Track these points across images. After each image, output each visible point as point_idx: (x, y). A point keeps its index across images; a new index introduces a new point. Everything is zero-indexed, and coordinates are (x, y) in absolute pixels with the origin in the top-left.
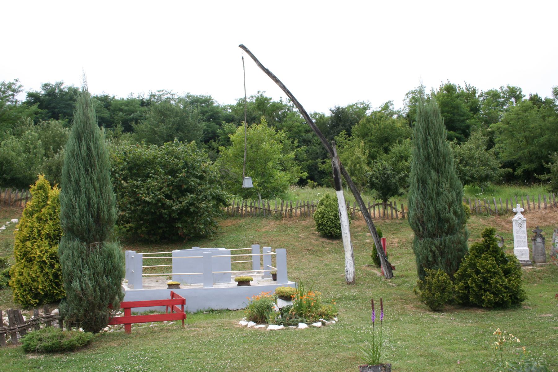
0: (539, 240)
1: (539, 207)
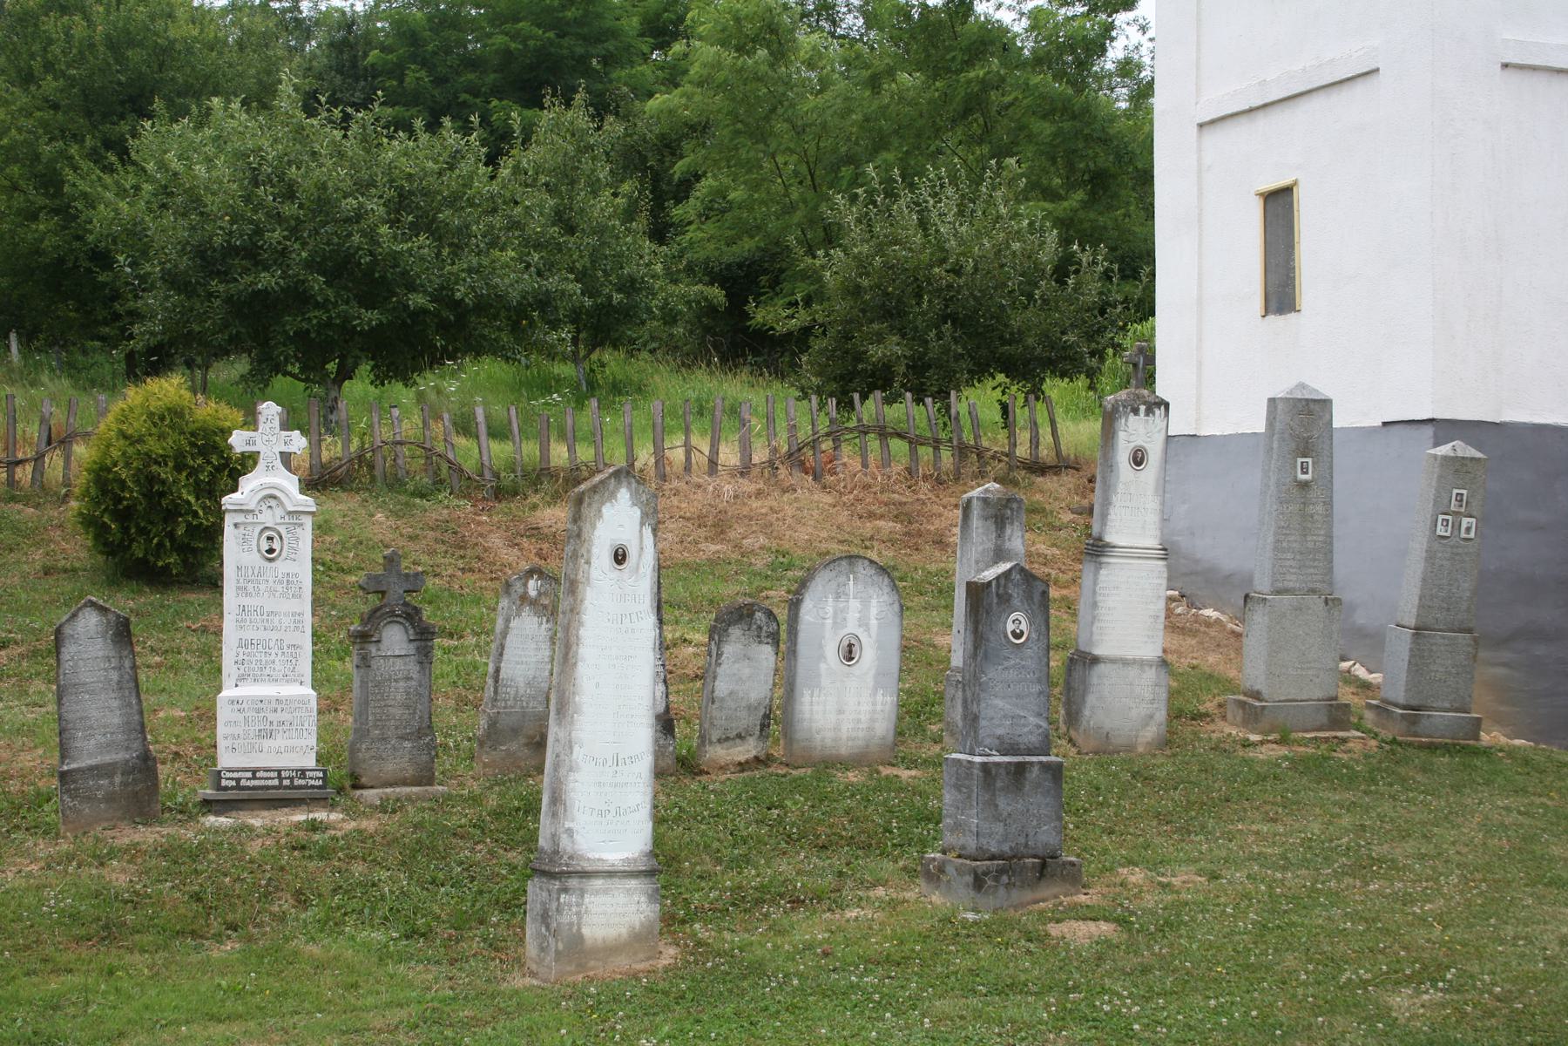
0: (395, 639)
1: (713, 463)
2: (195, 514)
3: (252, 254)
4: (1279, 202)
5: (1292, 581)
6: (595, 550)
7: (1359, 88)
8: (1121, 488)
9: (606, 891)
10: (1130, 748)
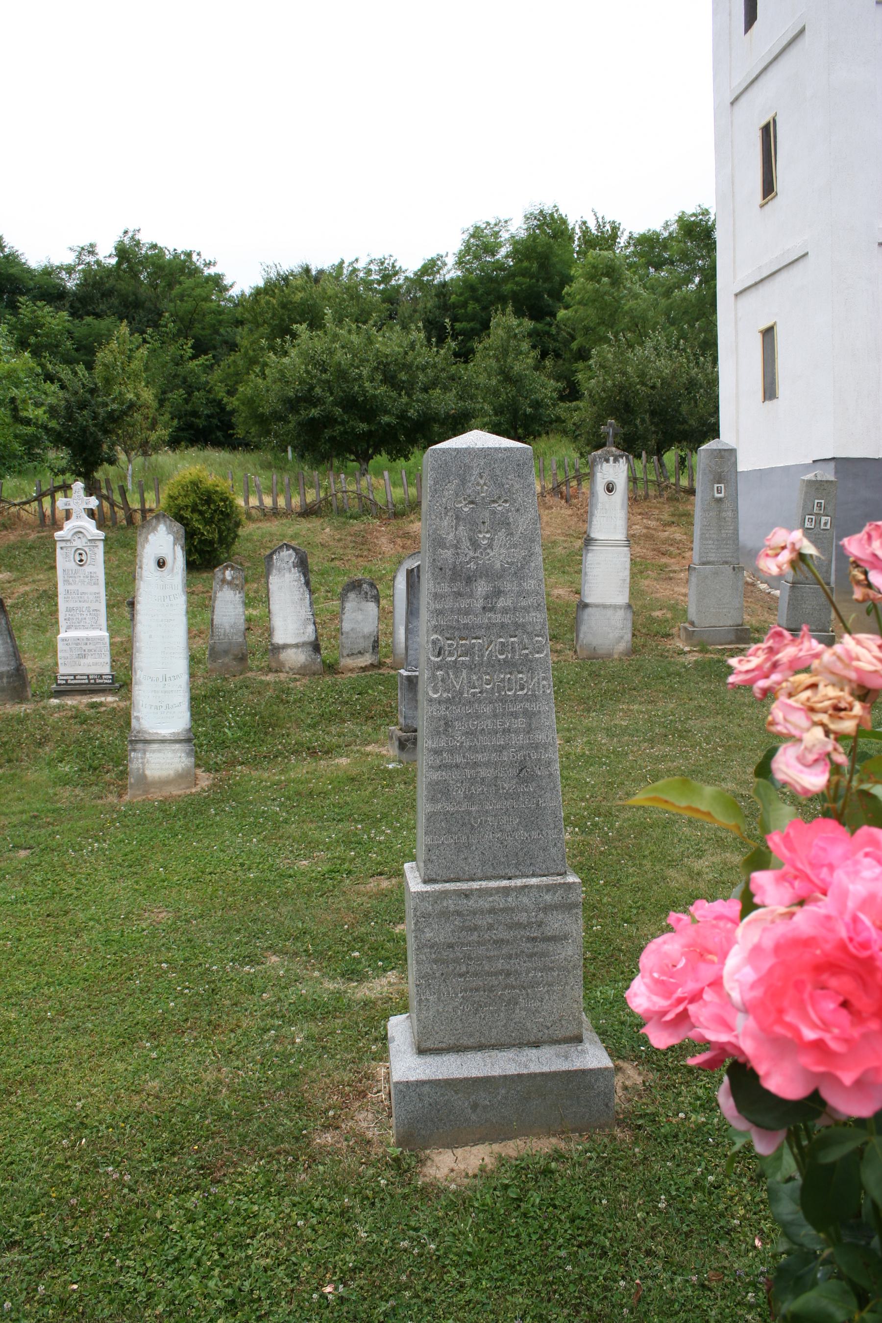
2: (203, 534)
3: (309, 399)
4: (768, 333)
5: (712, 557)
6: (145, 561)
7: (801, 265)
8: (600, 506)
9: (159, 751)
10: (610, 656)
